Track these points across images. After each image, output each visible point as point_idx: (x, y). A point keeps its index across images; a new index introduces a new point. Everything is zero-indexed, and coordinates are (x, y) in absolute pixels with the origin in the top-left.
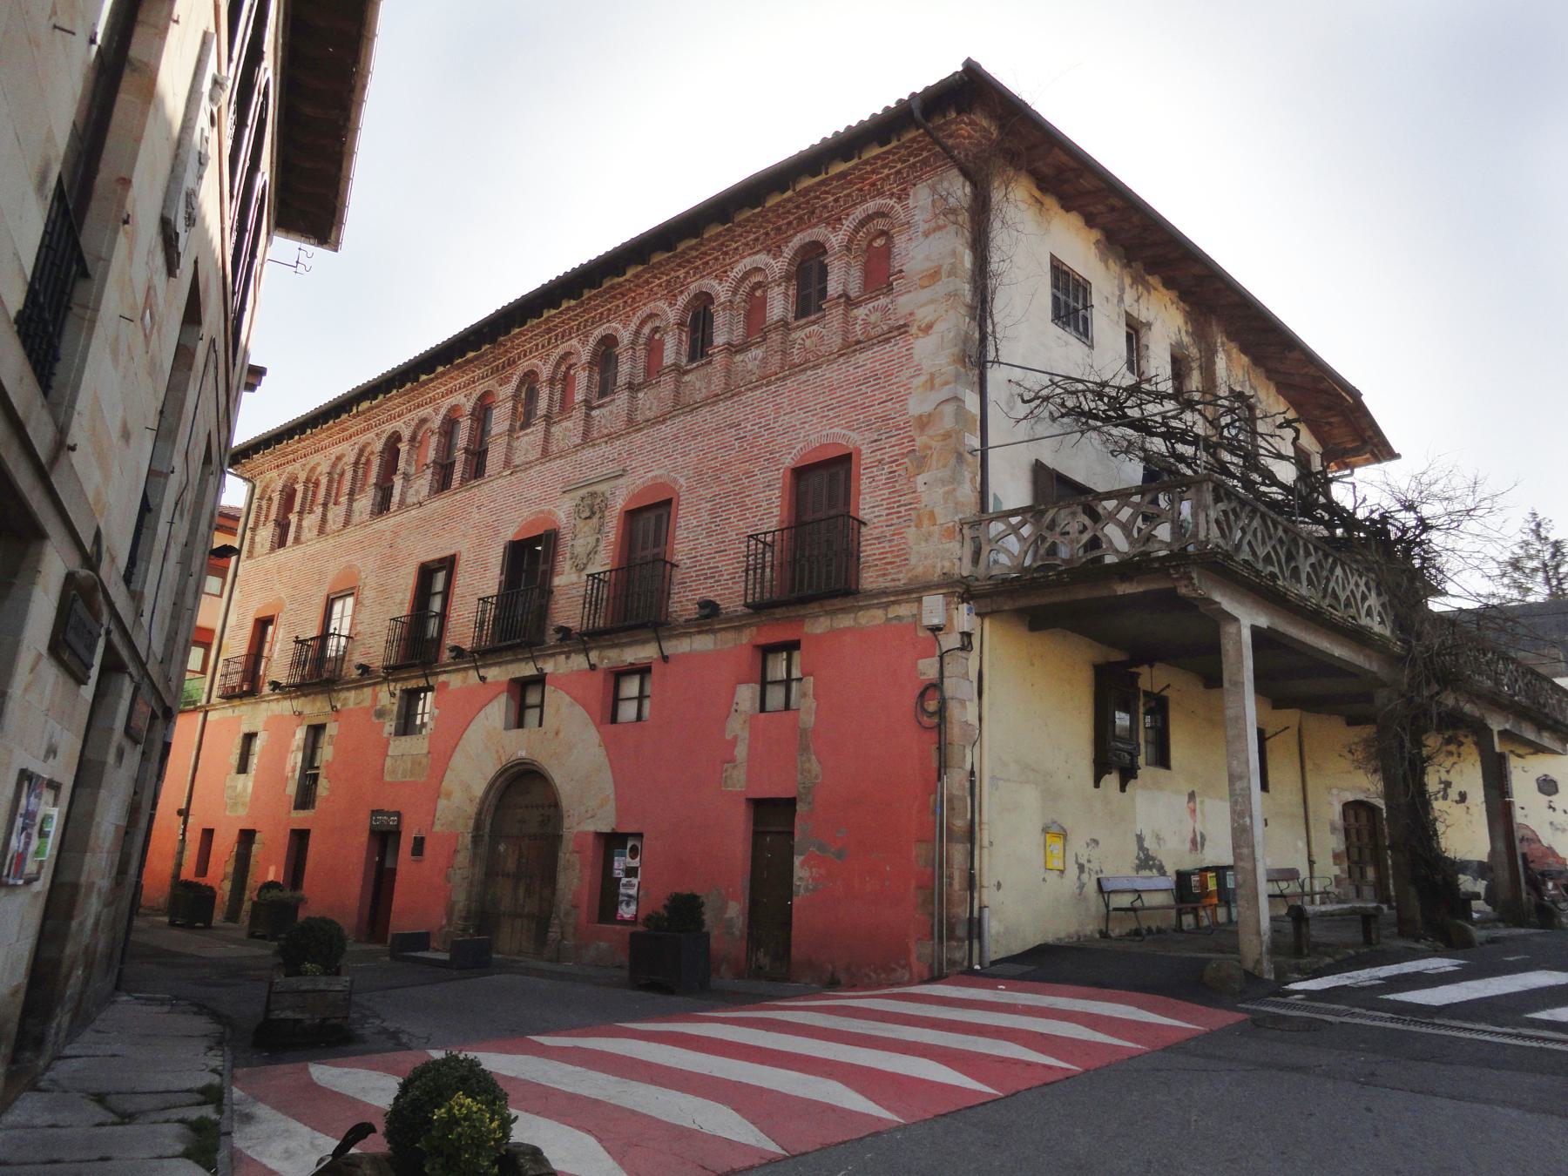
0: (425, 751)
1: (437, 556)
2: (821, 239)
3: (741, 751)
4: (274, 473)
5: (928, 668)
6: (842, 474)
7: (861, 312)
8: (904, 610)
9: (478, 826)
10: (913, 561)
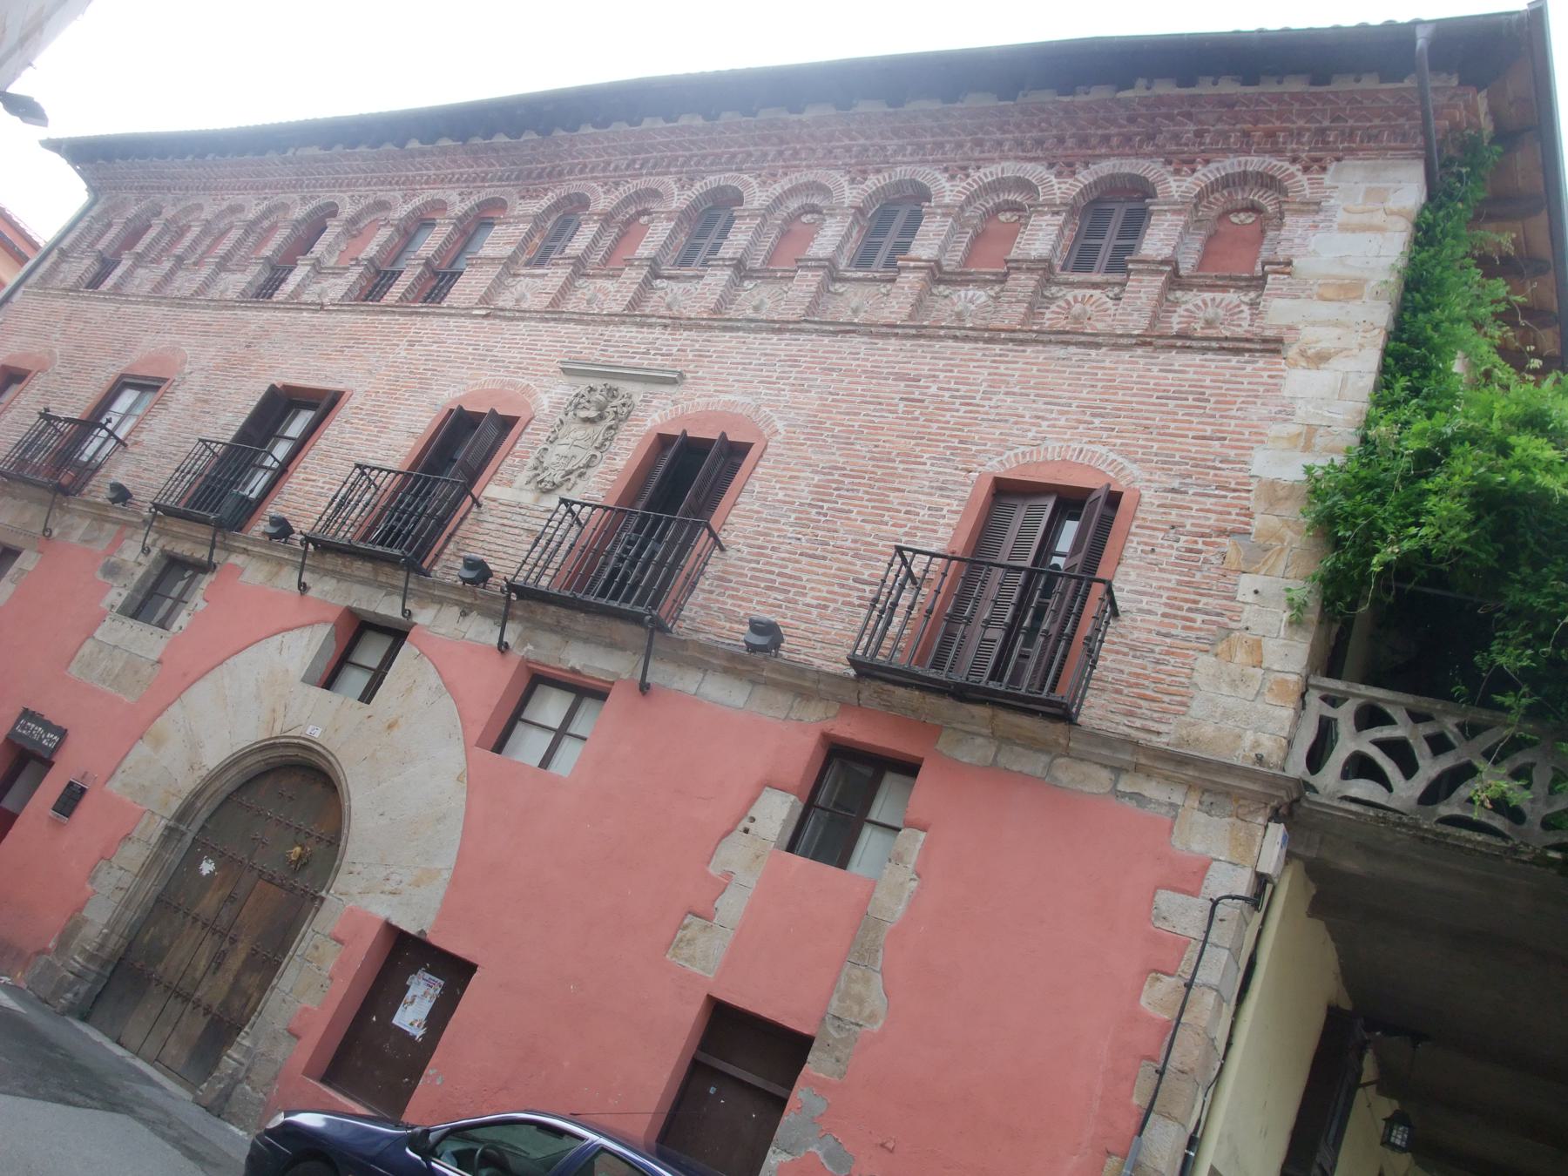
0: (154, 657)
2: (1151, 177)
3: (731, 907)
7: (1192, 300)
9: (183, 814)
10: (1197, 709)
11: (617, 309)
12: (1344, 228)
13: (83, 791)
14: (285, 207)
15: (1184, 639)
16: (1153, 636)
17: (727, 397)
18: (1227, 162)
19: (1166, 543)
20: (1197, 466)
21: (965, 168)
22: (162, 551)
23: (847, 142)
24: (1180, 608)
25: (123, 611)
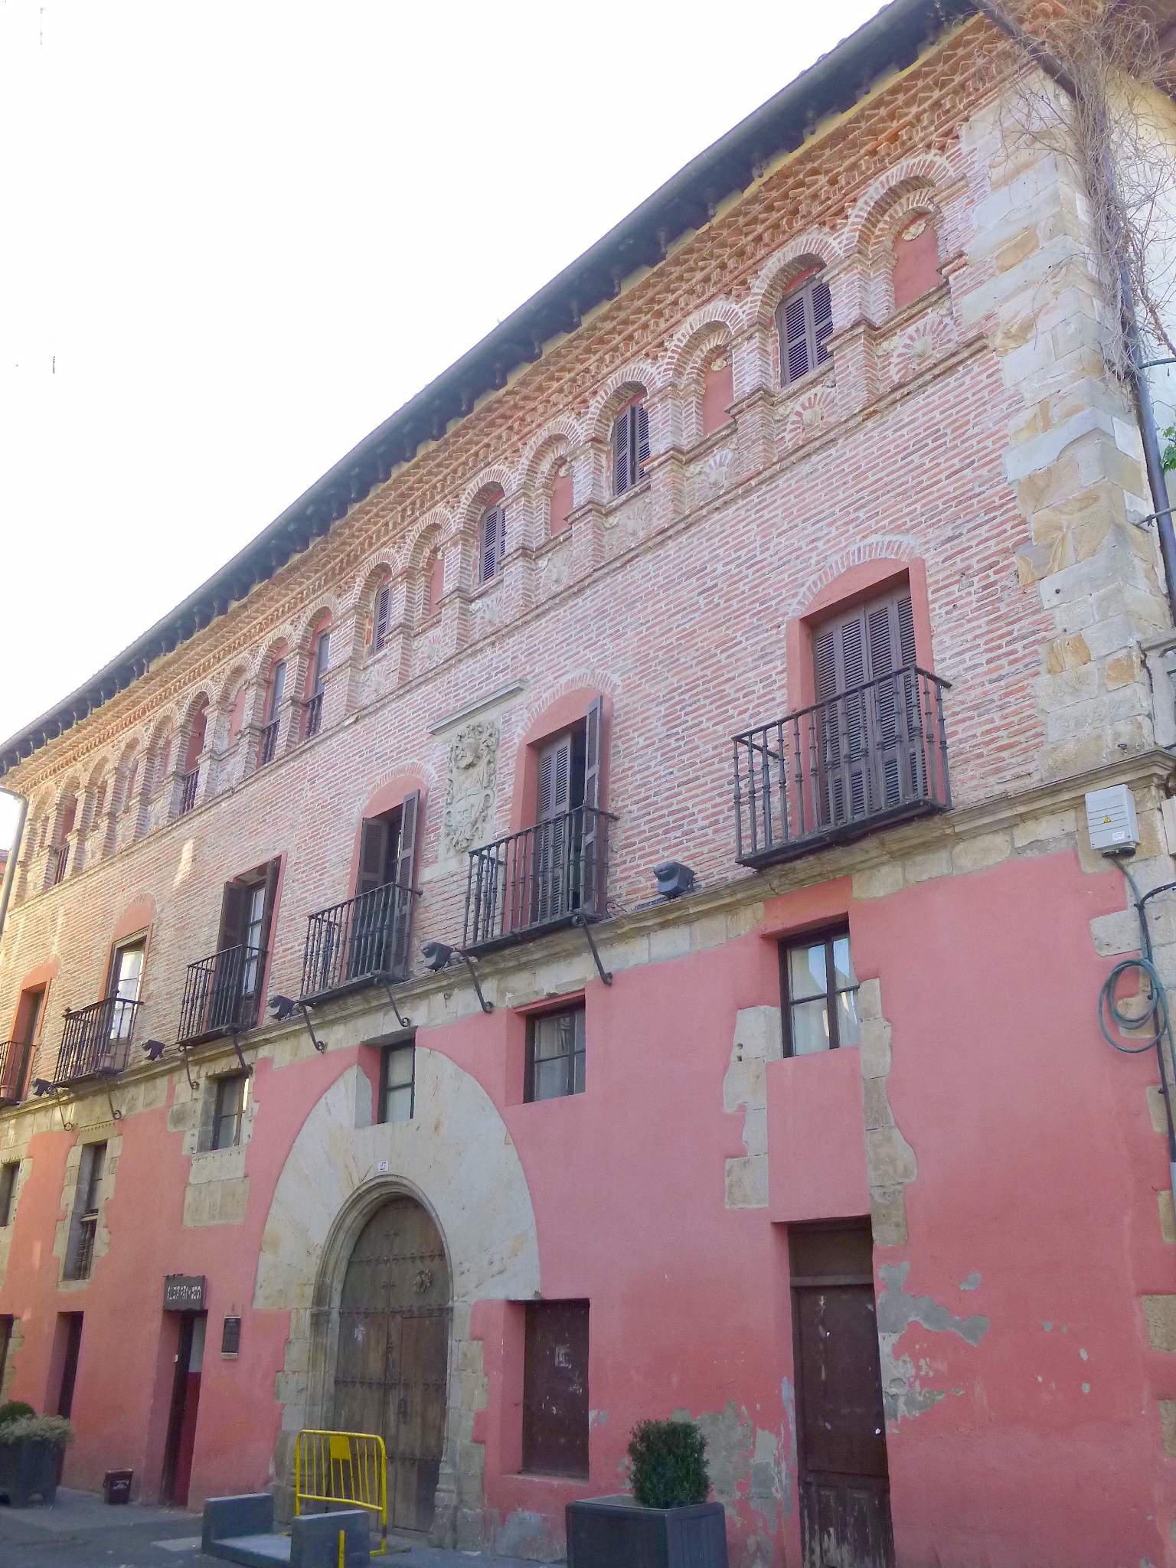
0: (240, 1174)
1: (256, 863)
2: (813, 249)
3: (755, 1134)
4: (50, 783)
5: (1116, 935)
6: (893, 612)
7: (896, 344)
8: (1047, 828)
9: (321, 1296)
10: (1053, 734)
11: (451, 651)
12: (996, 186)
13: (238, 1321)
14: (167, 719)
15: (1015, 673)
16: (988, 687)
17: (563, 680)
18: (871, 189)
19: (963, 593)
20: (960, 503)
21: (662, 344)
22: (208, 1077)
23: (556, 385)
24: (1000, 647)
25: (202, 1148)
